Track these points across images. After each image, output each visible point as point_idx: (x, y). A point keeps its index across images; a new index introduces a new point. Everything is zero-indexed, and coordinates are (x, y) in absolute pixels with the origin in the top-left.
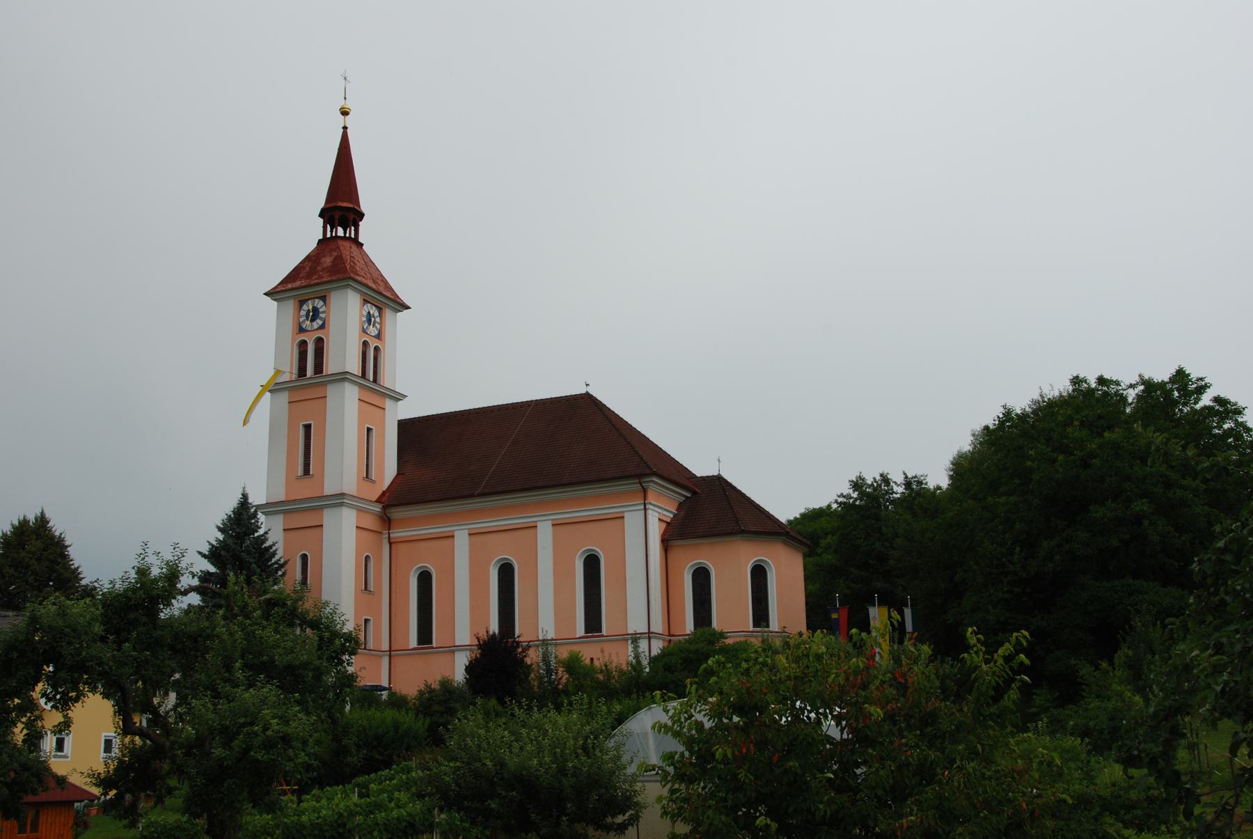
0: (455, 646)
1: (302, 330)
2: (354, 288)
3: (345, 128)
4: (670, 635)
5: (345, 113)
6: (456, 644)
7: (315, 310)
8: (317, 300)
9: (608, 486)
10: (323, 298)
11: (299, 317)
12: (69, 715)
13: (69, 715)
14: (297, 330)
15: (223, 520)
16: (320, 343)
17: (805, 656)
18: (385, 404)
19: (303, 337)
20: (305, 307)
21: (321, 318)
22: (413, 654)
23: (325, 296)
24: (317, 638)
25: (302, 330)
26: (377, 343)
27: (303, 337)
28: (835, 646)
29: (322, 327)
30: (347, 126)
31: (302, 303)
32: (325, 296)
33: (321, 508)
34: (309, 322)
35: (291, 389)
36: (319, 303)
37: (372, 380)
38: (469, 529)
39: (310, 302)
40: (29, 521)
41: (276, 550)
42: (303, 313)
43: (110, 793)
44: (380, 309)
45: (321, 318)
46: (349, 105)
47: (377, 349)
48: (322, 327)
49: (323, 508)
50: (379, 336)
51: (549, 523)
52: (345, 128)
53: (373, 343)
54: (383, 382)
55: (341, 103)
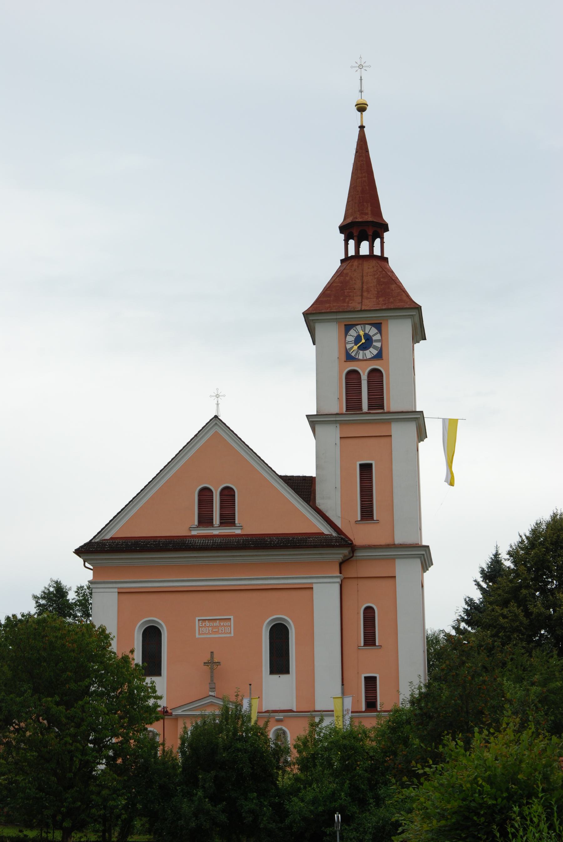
0: (315, 711)
1: (349, 358)
3: (362, 127)
5: (361, 108)
6: (316, 709)
7: (368, 338)
9: (264, 555)
10: (378, 326)
11: (346, 343)
14: (343, 357)
15: (488, 564)
17: (122, 745)
19: (352, 366)
20: (352, 332)
21: (375, 348)
22: (365, 717)
23: (381, 323)
25: (349, 358)
27: (352, 366)
28: (320, 752)
29: (379, 356)
30: (364, 125)
31: (348, 328)
32: (381, 323)
33: (393, 559)
34: (356, 347)
35: (342, 423)
36: (372, 331)
39: (359, 327)
42: (350, 339)
43: (399, 829)
45: (375, 348)
46: (366, 98)
48: (379, 356)
49: (394, 559)
52: (362, 127)
55: (356, 98)
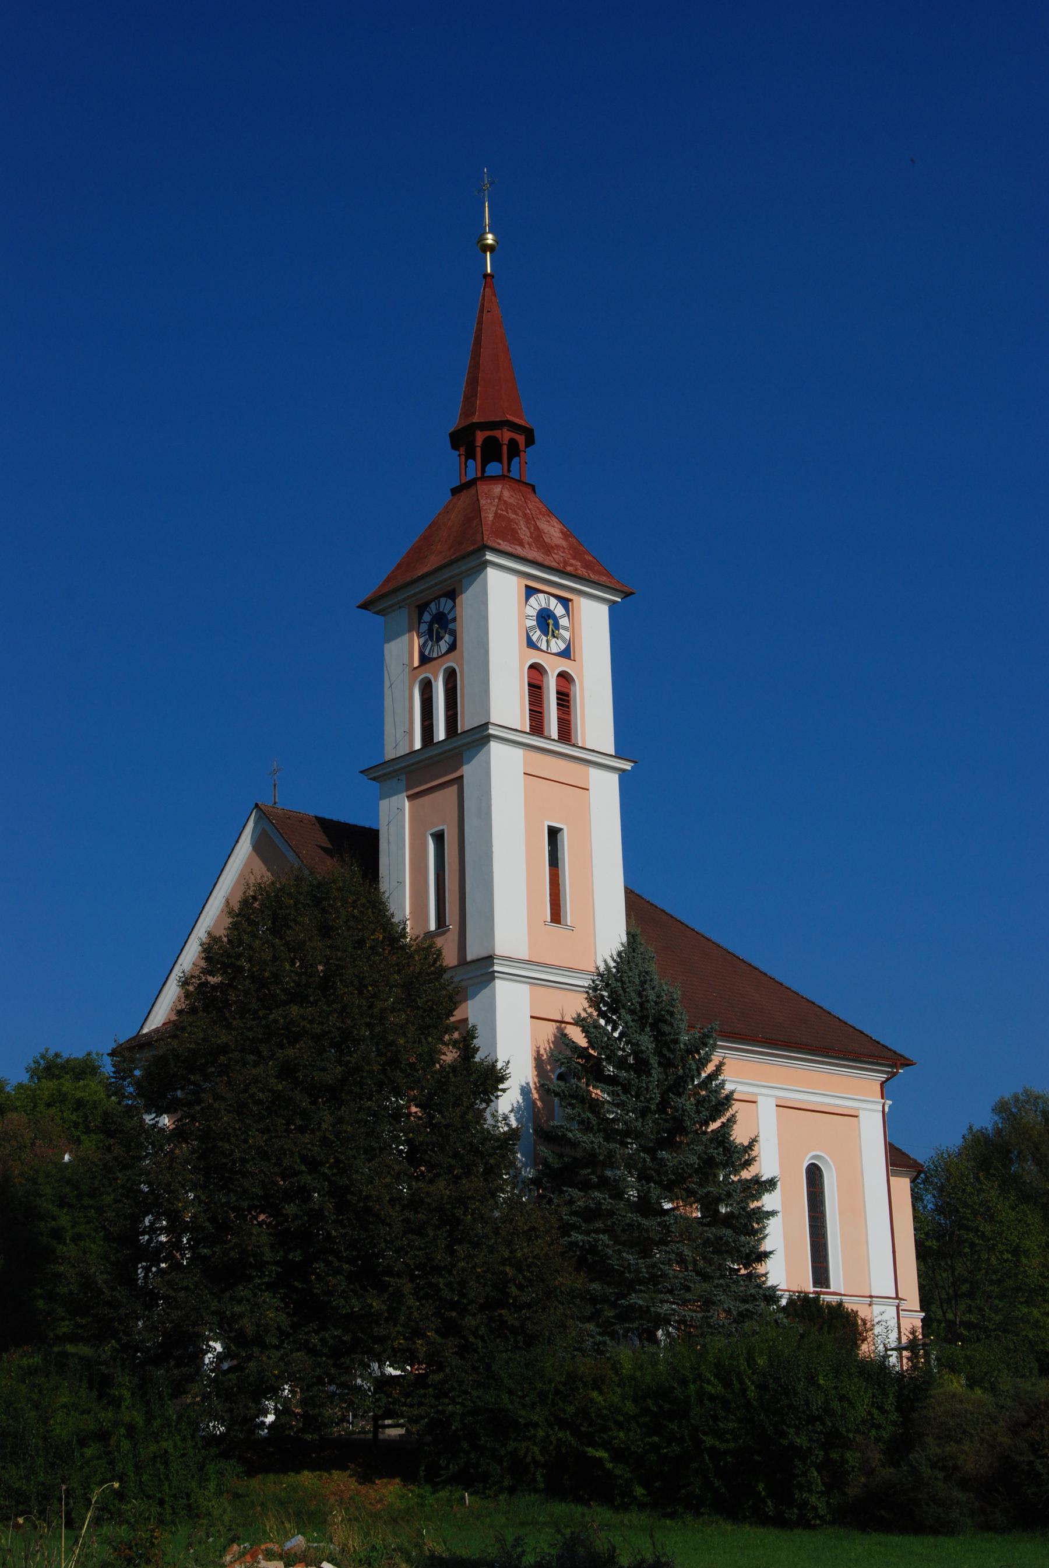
2: (474, 741)
4: (897, 1298)
8: (443, 600)
12: (113, 1069)
13: (113, 1069)
16: (451, 677)
18: (587, 777)
24: (417, 970)
26: (564, 665)
29: (453, 647)
37: (556, 738)
38: (777, 1098)
40: (748, 1163)
41: (733, 1116)
44: (565, 602)
47: (564, 676)
50: (566, 654)
51: (773, 1102)
53: (553, 667)
54: (584, 741)
